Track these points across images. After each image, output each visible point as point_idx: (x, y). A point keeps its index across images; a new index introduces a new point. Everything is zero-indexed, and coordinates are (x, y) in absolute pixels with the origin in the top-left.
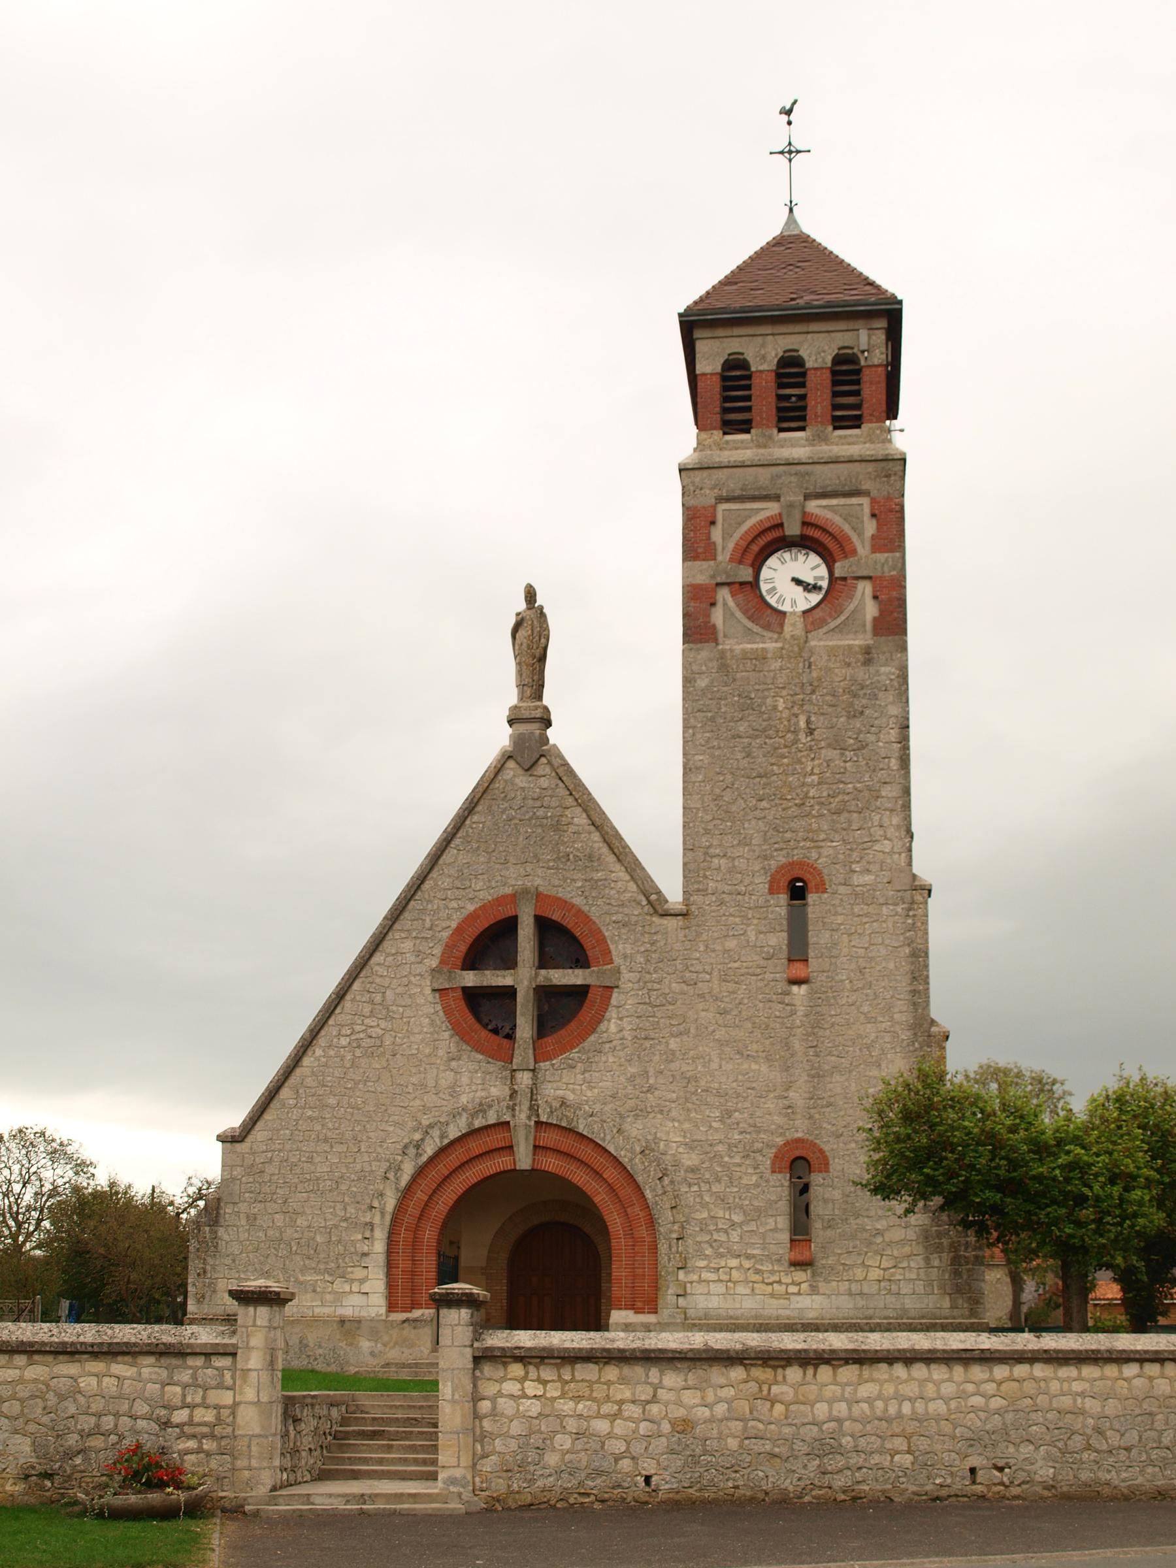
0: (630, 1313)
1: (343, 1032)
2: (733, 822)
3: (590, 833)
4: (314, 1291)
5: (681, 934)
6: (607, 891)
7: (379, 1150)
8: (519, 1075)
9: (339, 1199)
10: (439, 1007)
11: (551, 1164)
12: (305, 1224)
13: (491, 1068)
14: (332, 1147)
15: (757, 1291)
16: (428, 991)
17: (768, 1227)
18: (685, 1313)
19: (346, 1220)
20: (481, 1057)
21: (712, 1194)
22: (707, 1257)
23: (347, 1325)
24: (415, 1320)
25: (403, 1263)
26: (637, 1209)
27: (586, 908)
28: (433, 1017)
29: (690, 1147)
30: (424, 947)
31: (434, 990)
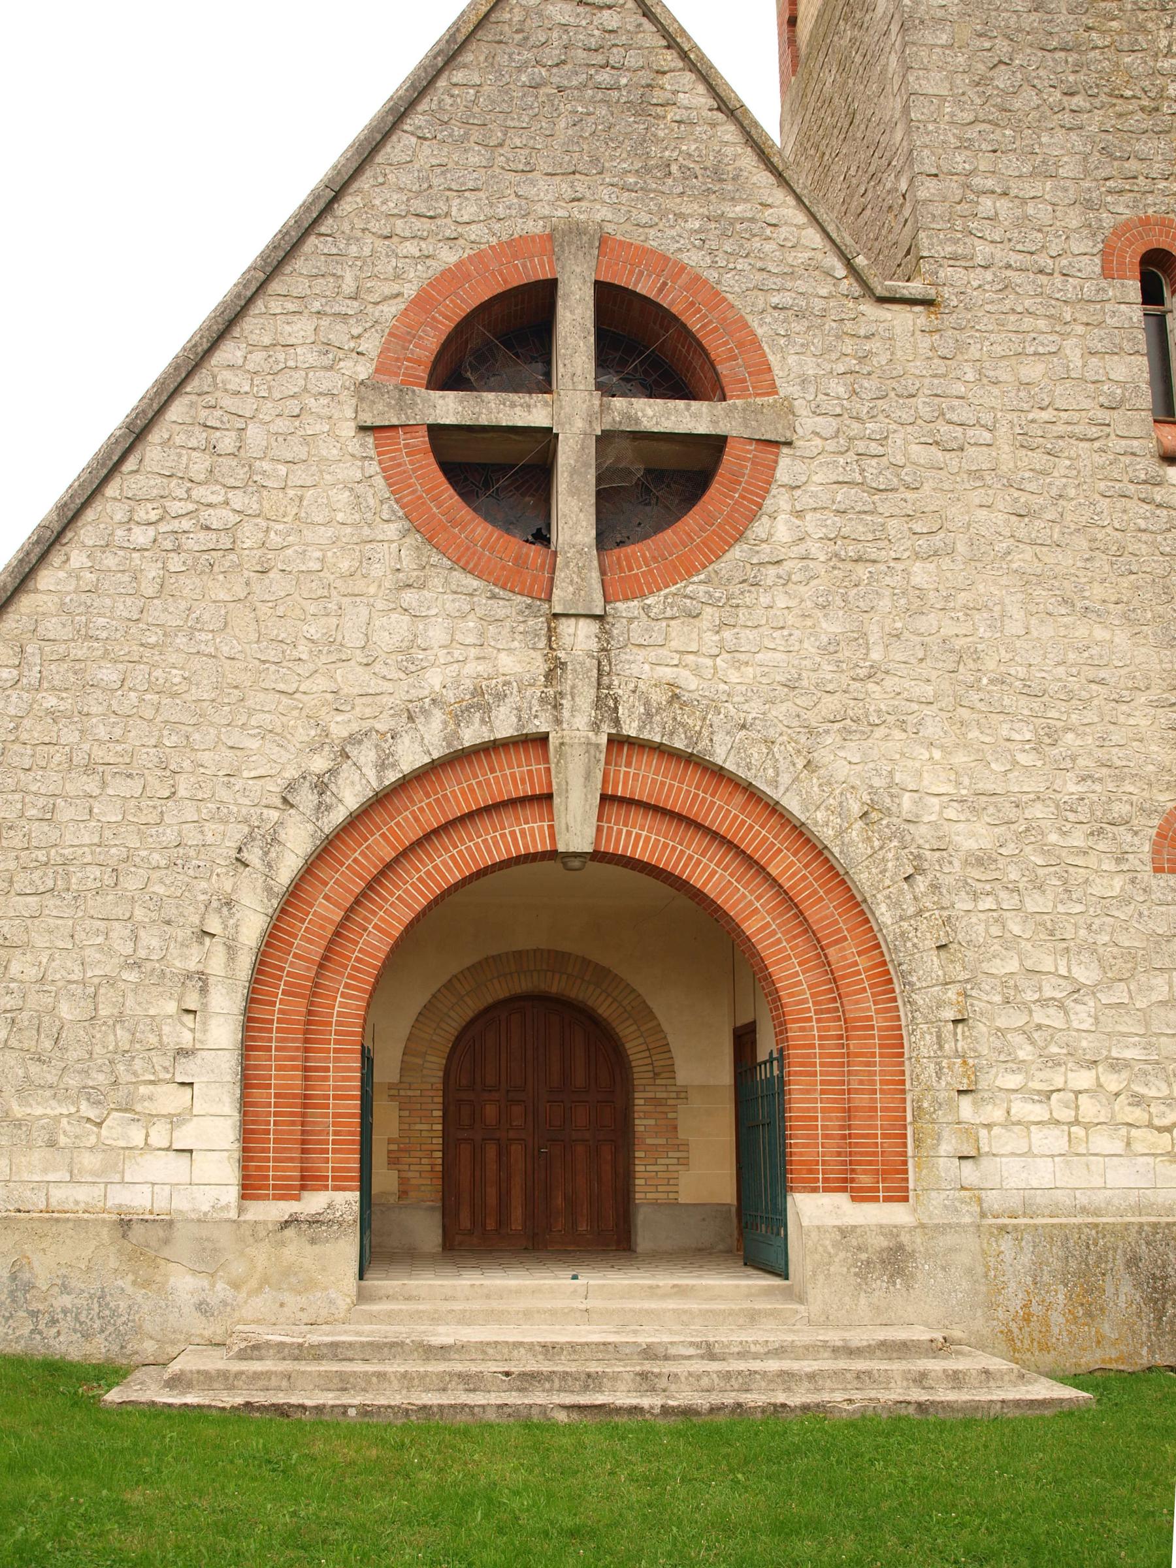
0: (841, 1200)
1: (141, 514)
2: (1018, 130)
3: (713, 125)
4: (52, 1144)
5: (925, 342)
6: (756, 243)
7: (223, 794)
8: (566, 627)
9: (119, 912)
10: (374, 468)
11: (641, 839)
12: (32, 973)
13: (500, 609)
14: (104, 784)
15: (1138, 1147)
16: (348, 430)
17: (1155, 997)
18: (980, 1201)
19: (137, 965)
20: (476, 583)
21: (1028, 917)
22: (1021, 1066)
23: (137, 1231)
24: (315, 1221)
25: (280, 1076)
26: (851, 949)
27: (712, 275)
28: (360, 489)
29: (974, 804)
30: (339, 334)
31: (363, 429)
